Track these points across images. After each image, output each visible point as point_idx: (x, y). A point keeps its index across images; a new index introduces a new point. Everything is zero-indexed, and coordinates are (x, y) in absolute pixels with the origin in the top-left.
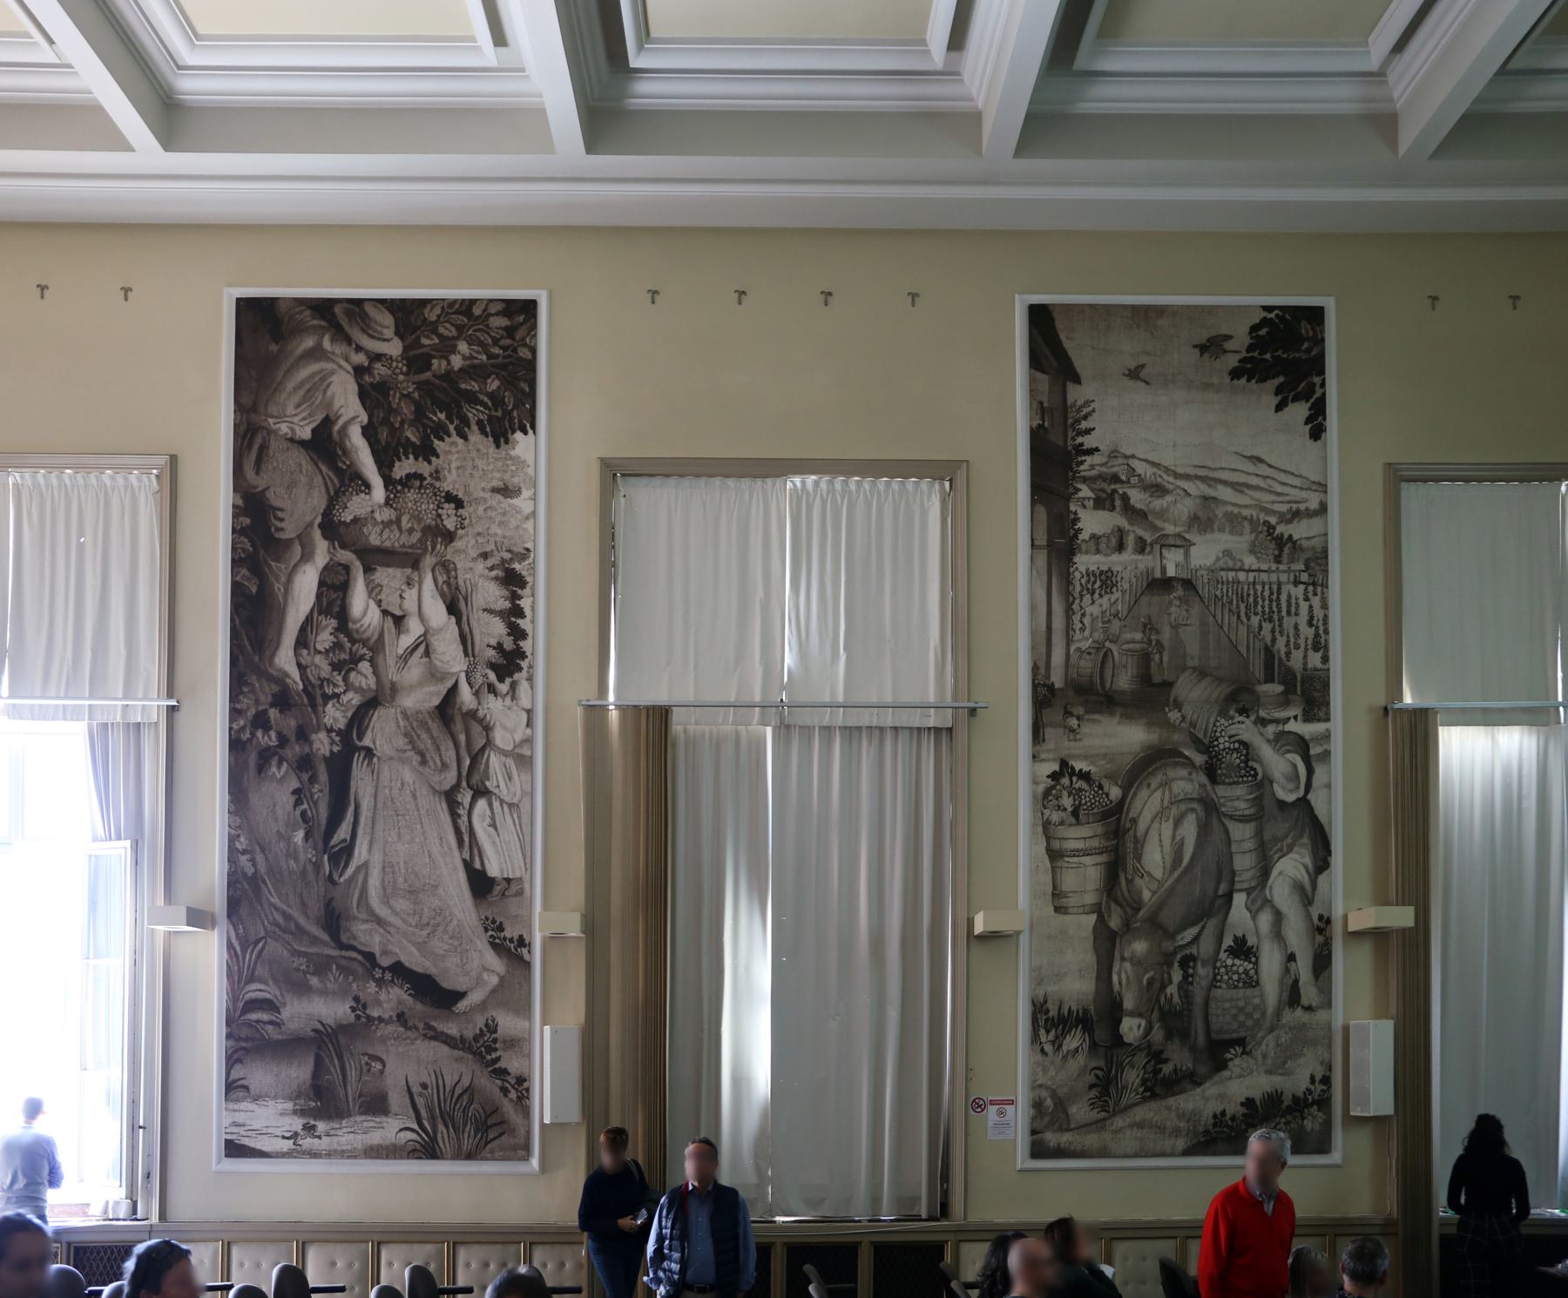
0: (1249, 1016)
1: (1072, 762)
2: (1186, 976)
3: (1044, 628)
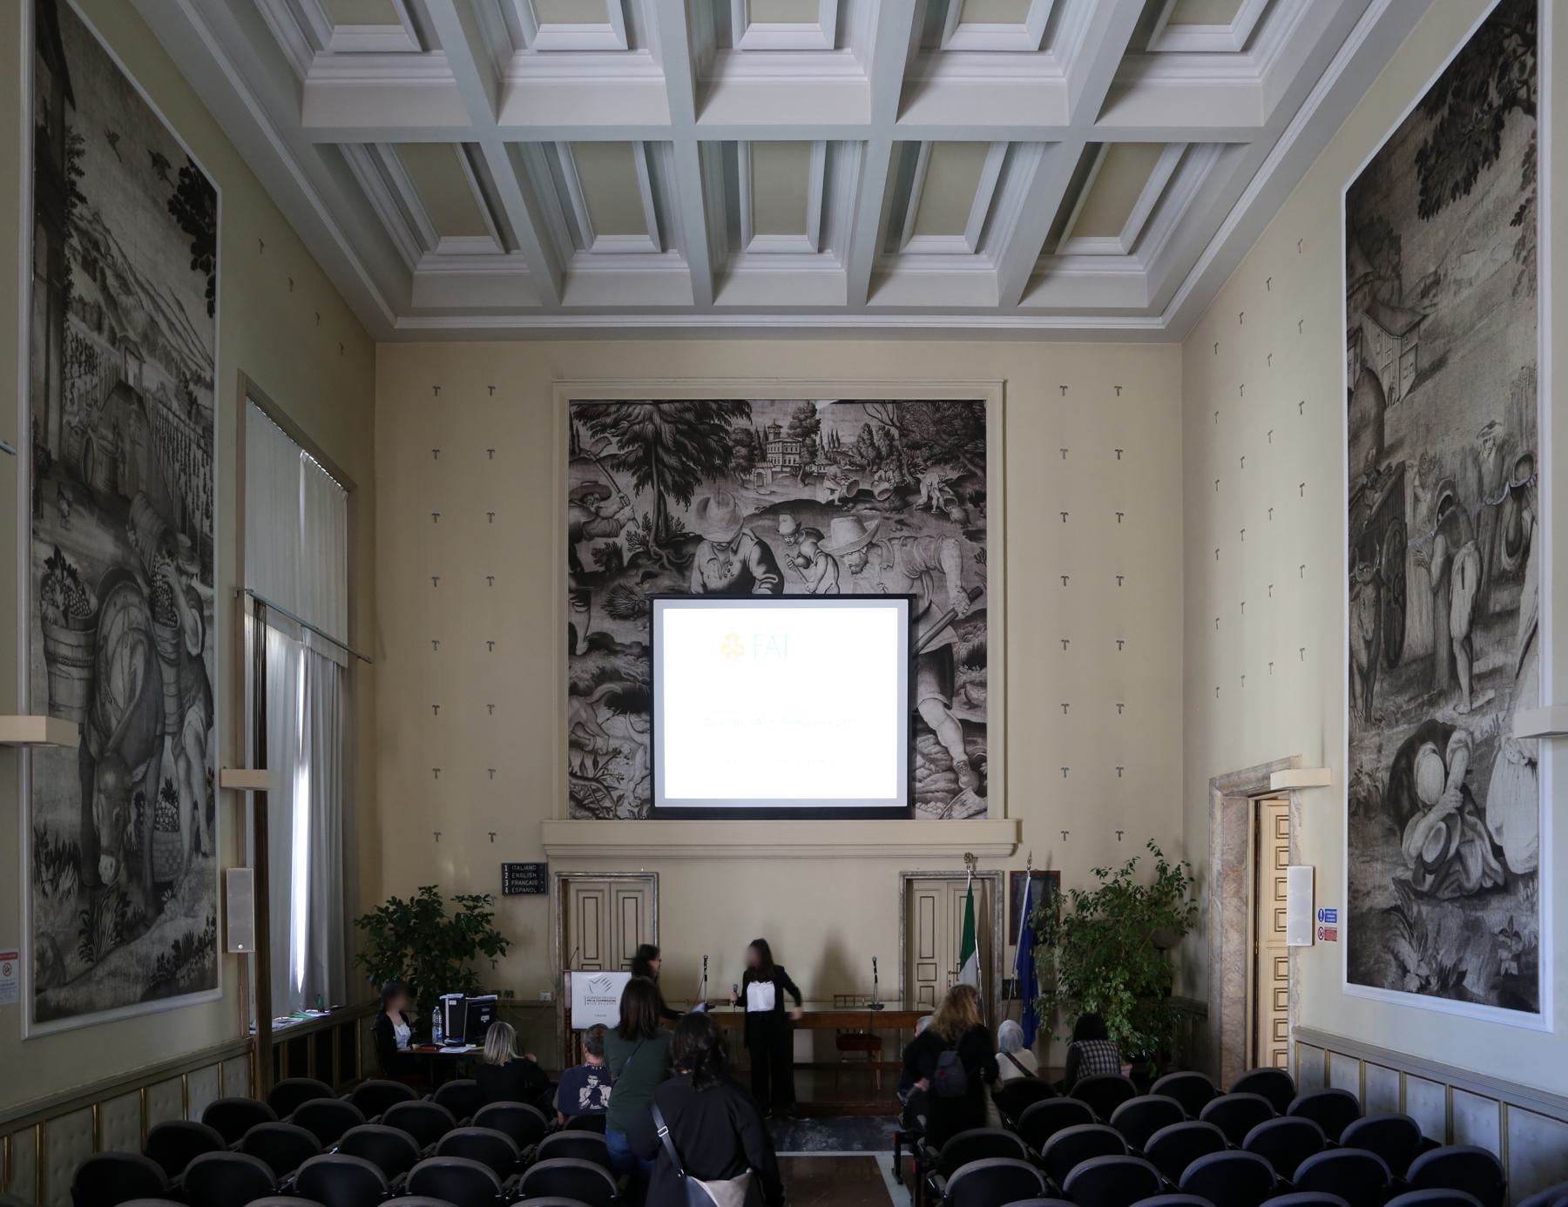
0: (175, 859)
1: (63, 554)
2: (139, 815)
3: (43, 379)
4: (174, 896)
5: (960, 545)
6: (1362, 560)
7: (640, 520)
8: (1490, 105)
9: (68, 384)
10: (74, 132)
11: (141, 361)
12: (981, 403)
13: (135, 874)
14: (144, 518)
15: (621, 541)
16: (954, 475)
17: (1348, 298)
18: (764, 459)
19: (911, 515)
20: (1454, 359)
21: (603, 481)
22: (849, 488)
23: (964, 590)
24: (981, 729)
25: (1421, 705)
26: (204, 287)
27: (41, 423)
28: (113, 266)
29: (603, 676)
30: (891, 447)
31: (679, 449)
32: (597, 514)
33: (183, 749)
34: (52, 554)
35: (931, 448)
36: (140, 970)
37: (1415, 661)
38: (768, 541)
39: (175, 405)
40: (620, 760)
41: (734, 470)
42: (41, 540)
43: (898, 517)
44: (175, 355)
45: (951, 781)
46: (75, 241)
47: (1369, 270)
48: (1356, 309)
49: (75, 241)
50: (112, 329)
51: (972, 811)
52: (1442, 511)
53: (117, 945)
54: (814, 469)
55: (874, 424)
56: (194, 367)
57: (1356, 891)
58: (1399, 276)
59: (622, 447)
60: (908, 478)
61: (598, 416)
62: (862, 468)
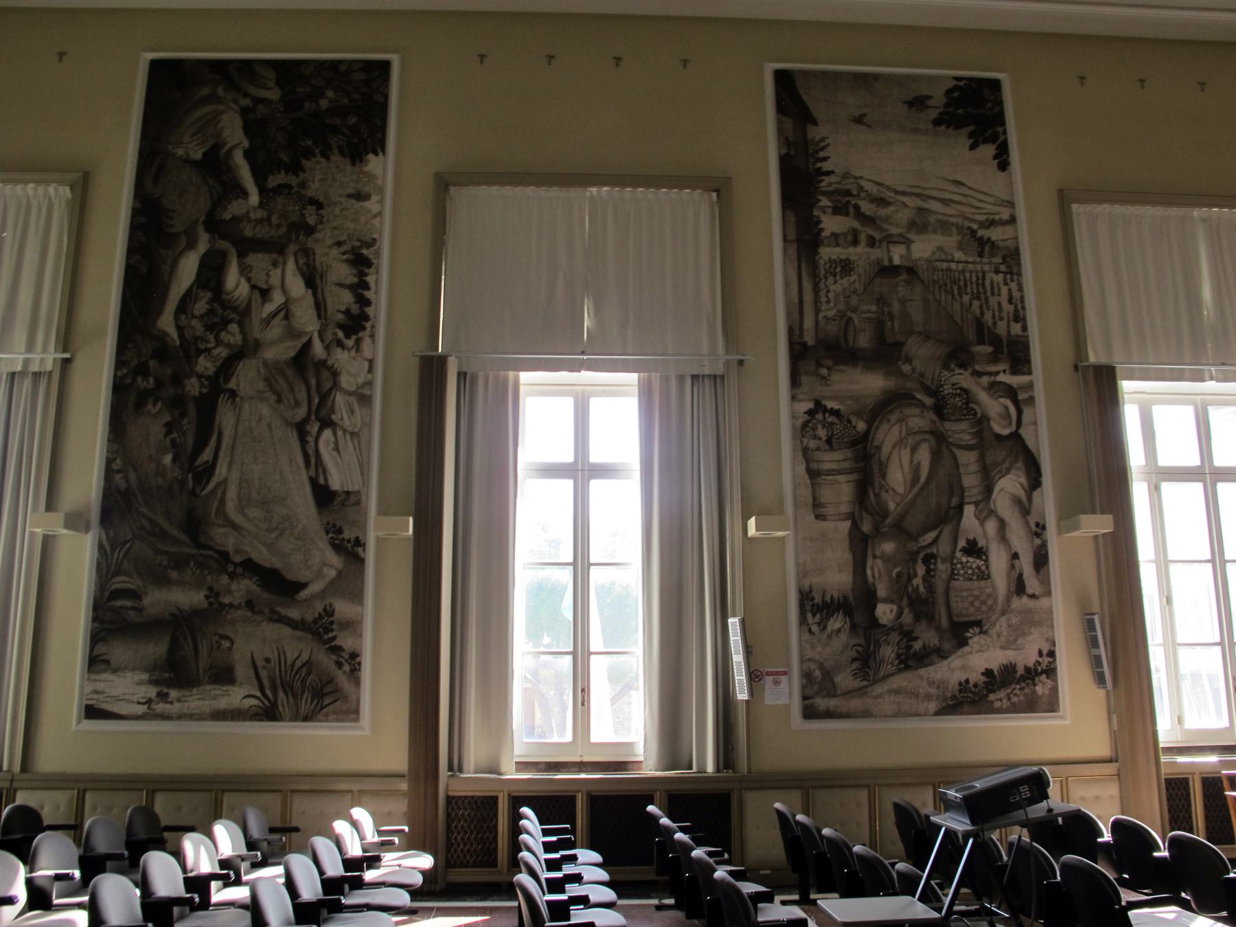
0: (983, 602)
1: (824, 402)
46: (825, 202)
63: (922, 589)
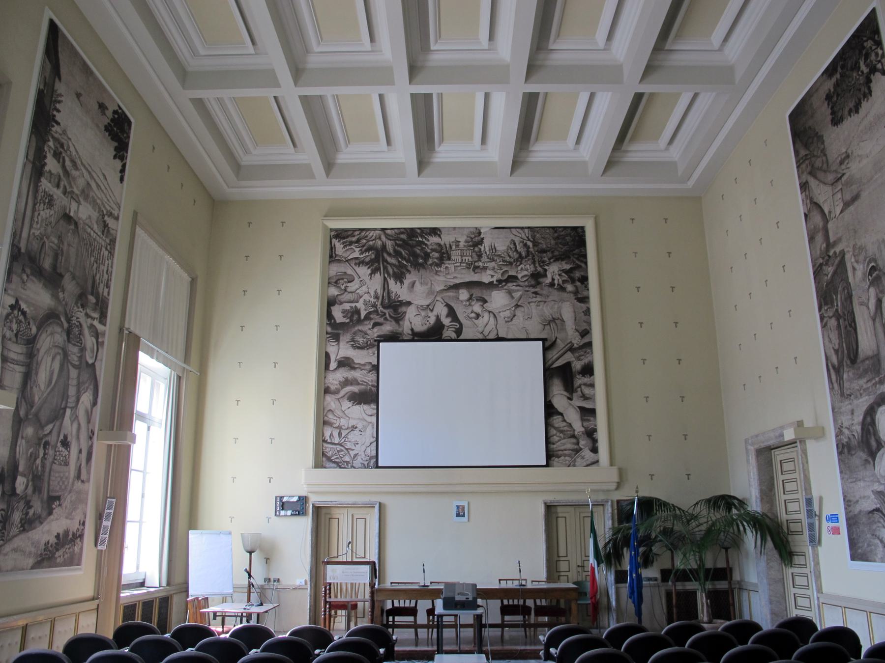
0: (63, 483)
1: (20, 302)
2: (45, 454)
3: (23, 211)
4: (60, 505)
5: (574, 307)
6: (826, 304)
7: (372, 293)
8: (862, 72)
9: (36, 214)
10: (59, 92)
11: (79, 203)
12: (583, 228)
13: (37, 489)
14: (70, 286)
15: (360, 305)
16: (568, 267)
17: (798, 167)
18: (449, 259)
19: (542, 289)
20: (864, 195)
21: (350, 271)
22: (502, 275)
23: (577, 330)
24: (592, 412)
25: (875, 384)
26: (120, 168)
27: (18, 233)
28: (70, 156)
29: (347, 382)
30: (528, 253)
31: (397, 254)
32: (345, 290)
33: (77, 417)
34: (13, 302)
35: (553, 252)
36: (33, 550)
37: (867, 359)
38: (452, 305)
39: (95, 227)
40: (357, 432)
41: (431, 265)
42: (9, 294)
43: (533, 290)
44: (98, 201)
45: (574, 444)
46: (51, 143)
47: (808, 152)
48: (803, 173)
49: (51, 143)
50: (65, 187)
51: (589, 462)
52: (870, 274)
53: (21, 532)
54: (481, 264)
55: (517, 240)
56: (109, 208)
57: (849, 501)
58: (825, 155)
59: (362, 253)
60: (539, 269)
61: (347, 237)
62: (511, 264)
63: (40, 468)
